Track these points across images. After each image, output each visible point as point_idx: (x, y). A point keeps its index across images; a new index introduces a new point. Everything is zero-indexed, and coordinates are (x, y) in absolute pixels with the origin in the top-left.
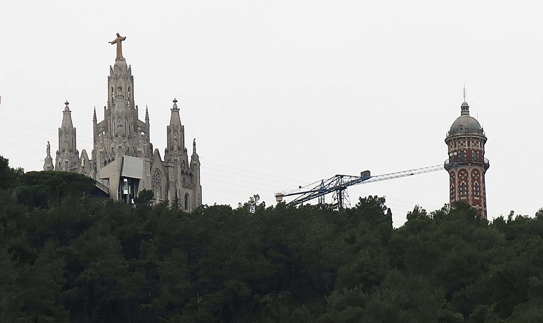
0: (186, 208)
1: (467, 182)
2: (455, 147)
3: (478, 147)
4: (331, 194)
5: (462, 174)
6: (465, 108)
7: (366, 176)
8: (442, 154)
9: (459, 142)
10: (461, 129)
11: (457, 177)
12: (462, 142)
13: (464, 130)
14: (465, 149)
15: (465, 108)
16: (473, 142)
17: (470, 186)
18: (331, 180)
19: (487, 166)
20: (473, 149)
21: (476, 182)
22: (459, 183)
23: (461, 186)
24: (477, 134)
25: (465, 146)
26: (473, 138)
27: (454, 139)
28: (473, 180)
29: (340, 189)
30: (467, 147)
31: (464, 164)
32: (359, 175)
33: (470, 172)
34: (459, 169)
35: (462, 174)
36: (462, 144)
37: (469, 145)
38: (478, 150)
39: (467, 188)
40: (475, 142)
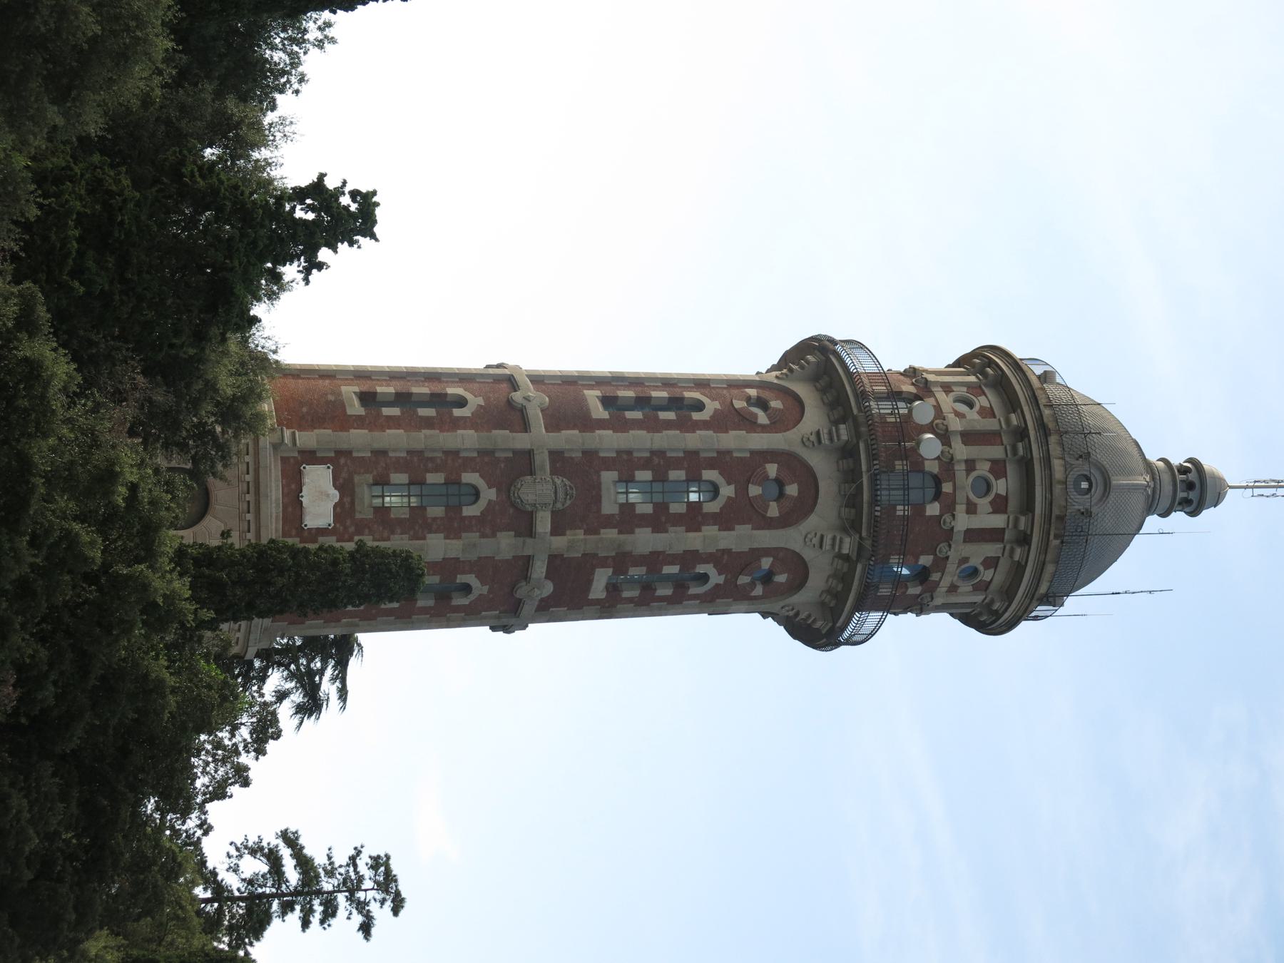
0: (294, 434)
5: (780, 483)
6: (1192, 489)
12: (1000, 487)
13: (1079, 502)
14: (949, 508)
15: (1192, 489)
16: (991, 563)
20: (941, 563)
21: (716, 578)
25: (971, 509)
27: (1021, 434)
31: (852, 501)
33: (791, 538)
34: (808, 554)
35: (780, 483)
37: (974, 536)
39: (672, 559)
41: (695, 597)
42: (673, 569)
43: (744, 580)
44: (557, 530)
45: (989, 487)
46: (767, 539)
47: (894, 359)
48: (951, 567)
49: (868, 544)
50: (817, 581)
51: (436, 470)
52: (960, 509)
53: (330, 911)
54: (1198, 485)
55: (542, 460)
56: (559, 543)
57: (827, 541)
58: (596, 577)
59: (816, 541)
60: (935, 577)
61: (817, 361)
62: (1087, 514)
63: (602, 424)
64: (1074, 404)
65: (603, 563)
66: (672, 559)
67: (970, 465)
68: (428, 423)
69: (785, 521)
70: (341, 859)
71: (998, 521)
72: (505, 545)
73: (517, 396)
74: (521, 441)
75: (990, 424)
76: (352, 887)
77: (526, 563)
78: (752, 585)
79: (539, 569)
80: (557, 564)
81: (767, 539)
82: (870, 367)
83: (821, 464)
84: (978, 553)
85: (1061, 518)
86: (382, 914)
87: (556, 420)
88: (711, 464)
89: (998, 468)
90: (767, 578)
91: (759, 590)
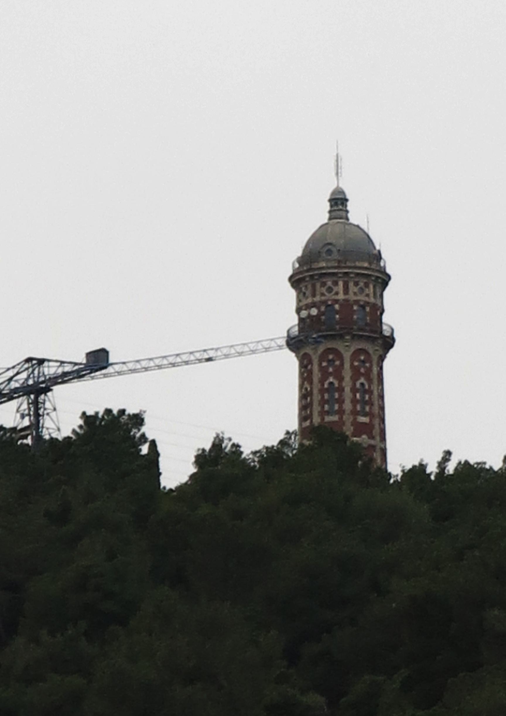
1: (341, 379)
2: (314, 295)
3: (368, 295)
5: (329, 361)
6: (338, 202)
8: (284, 313)
9: (324, 284)
12: (329, 283)
14: (336, 301)
15: (338, 202)
16: (356, 284)
17: (315, 391)
19: (388, 343)
20: (357, 302)
21: (362, 380)
23: (327, 390)
24: (366, 265)
25: (337, 293)
26: (358, 274)
27: (312, 277)
28: (356, 374)
29: (37, 391)
32: (83, 359)
33: (347, 356)
34: (352, 349)
35: (329, 361)
36: (330, 290)
37: (346, 291)
40: (361, 284)
41: (370, 387)
42: (358, 395)
43: (362, 370)
45: (332, 290)
46: (347, 365)
48: (358, 298)
49: (345, 331)
52: (336, 297)
54: (336, 201)
57: (347, 344)
58: (361, 421)
59: (347, 348)
60: (362, 303)
64: (304, 251)
65: (355, 419)
66: (341, 396)
69: (340, 357)
71: (341, 283)
75: (310, 287)
78: (365, 367)
81: (347, 365)
82: (296, 328)
83: (321, 349)
84: (352, 288)
85: (339, 262)
88: (323, 385)
90: (363, 362)
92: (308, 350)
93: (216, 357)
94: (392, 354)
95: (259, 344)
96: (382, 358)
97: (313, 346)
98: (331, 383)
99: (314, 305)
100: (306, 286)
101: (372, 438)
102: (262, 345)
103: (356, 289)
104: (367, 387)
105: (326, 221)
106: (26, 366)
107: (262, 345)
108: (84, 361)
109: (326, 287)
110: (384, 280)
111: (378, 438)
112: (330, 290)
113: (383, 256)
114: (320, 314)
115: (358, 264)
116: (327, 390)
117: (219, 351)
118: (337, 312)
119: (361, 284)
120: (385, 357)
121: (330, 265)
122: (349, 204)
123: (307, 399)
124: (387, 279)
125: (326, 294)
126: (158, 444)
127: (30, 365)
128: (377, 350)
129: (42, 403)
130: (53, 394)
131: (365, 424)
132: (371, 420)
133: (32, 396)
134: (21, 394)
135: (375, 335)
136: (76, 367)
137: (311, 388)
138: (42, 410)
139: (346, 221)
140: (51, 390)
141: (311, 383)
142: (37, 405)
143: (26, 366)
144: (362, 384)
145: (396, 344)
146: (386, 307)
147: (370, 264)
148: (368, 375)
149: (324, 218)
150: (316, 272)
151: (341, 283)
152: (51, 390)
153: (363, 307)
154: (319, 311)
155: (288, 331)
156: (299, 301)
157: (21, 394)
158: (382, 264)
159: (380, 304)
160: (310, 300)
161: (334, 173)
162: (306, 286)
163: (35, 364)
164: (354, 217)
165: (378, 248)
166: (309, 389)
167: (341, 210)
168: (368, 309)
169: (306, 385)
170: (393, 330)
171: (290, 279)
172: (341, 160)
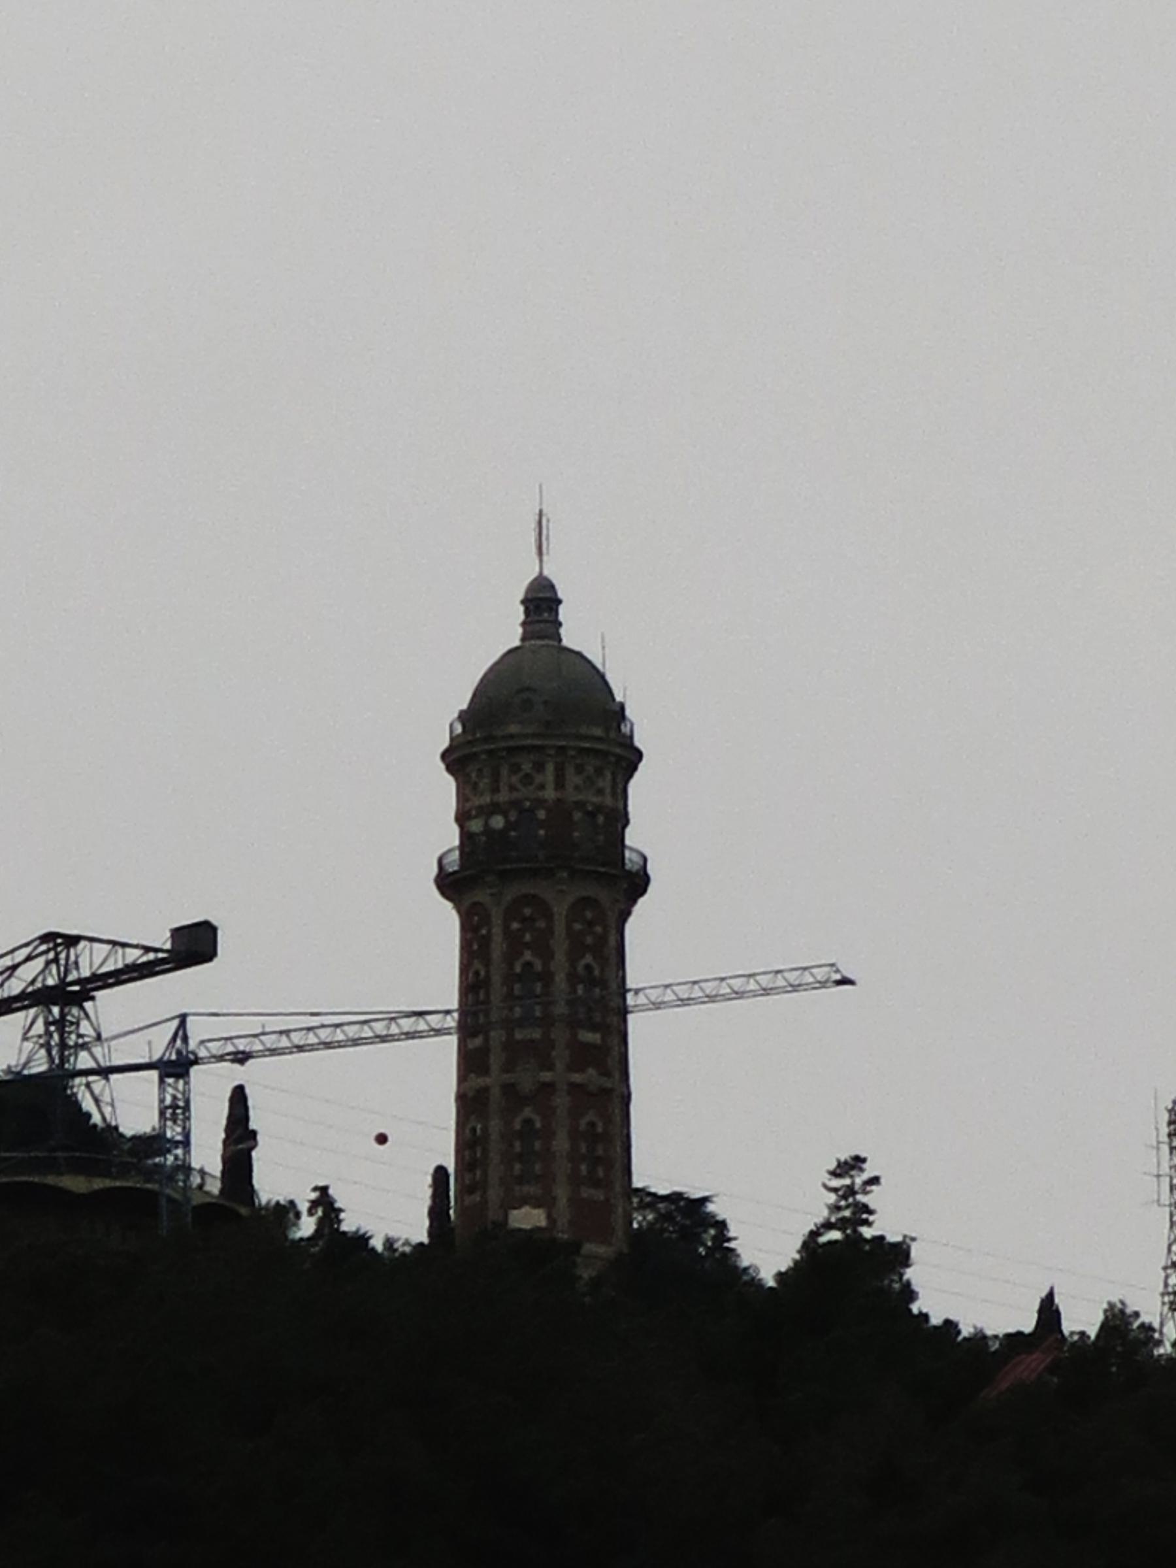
1: (546, 954)
2: (495, 790)
3: (600, 792)
4: (19, 1019)
6: (542, 604)
7: (195, 945)
8: (430, 818)
9: (515, 769)
10: (527, 705)
11: (497, 931)
12: (527, 767)
14: (540, 803)
15: (542, 604)
16: (580, 769)
17: (496, 979)
18: (25, 952)
19: (638, 883)
20: (580, 805)
21: (588, 959)
22: (511, 957)
23: (519, 978)
24: (598, 732)
25: (542, 787)
26: (582, 751)
27: (490, 752)
28: (577, 948)
29: (64, 998)
30: (550, 794)
32: (164, 941)
33: (560, 910)
34: (570, 899)
35: (524, 920)
36: (527, 779)
37: (560, 784)
38: (599, 809)
40: (590, 769)
41: (602, 971)
44: (551, 1068)
45: (527, 775)
46: (560, 928)
47: (452, 837)
50: (589, 890)
51: (511, 1146)
53: (866, 1209)
55: (507, 1078)
56: (559, 1066)
61: (449, 884)
62: (545, 703)
63: (487, 1040)
67: (512, 788)
68: (485, 1151)
69: (549, 916)
70: (832, 1198)
71: (550, 768)
72: (561, 1101)
73: (470, 1094)
74: (496, 1092)
76: (850, 1191)
77: (574, 1087)
79: (577, 1078)
80: (576, 1065)
81: (560, 928)
84: (573, 779)
86: (869, 1172)
87: (484, 1070)
88: (511, 966)
89: (515, 769)
90: (590, 924)
91: (599, 929)
92: (481, 896)
93: (636, 1006)
94: (642, 906)
95: (724, 984)
96: (625, 914)
97: (494, 891)
98: (528, 965)
99: (494, 808)
100: (480, 770)
101: (607, 1074)
102: (730, 986)
103: (578, 780)
104: (597, 972)
105: (517, 643)
106: (43, 947)
107: (730, 986)
108: (168, 946)
109: (521, 774)
110: (620, 758)
111: (617, 1075)
112: (527, 779)
113: (628, 713)
114: (509, 826)
115: (584, 730)
116: (519, 978)
117: (641, 995)
118: (541, 825)
119: (590, 769)
120: (629, 913)
121: (529, 731)
122: (562, 609)
123: (477, 993)
124: (634, 758)
125: (519, 786)
126: (248, 1091)
127: (51, 945)
128: (617, 901)
129: (72, 1023)
130: (95, 1006)
131: (594, 1046)
132: (603, 1039)
133: (56, 1010)
134: (26, 1003)
135: (613, 872)
136: (151, 956)
137: (487, 972)
138: (73, 1037)
139: (556, 643)
140: (93, 998)
141: (487, 963)
142: (64, 1026)
143: (43, 947)
144: (588, 967)
145: (650, 889)
146: (631, 816)
147: (607, 730)
148: (599, 948)
149: (512, 637)
150: (503, 744)
151: (550, 768)
152: (93, 998)
153: (592, 815)
154: (507, 821)
155: (440, 861)
156: (462, 797)
157: (26, 1003)
158: (625, 729)
159: (621, 806)
160: (487, 799)
161: (534, 550)
162: (480, 770)
163: (60, 945)
164: (571, 637)
165: (619, 698)
166: (483, 973)
167: (547, 621)
168: (601, 819)
169: (477, 965)
170: (645, 859)
171: (444, 756)
172: (548, 521)
